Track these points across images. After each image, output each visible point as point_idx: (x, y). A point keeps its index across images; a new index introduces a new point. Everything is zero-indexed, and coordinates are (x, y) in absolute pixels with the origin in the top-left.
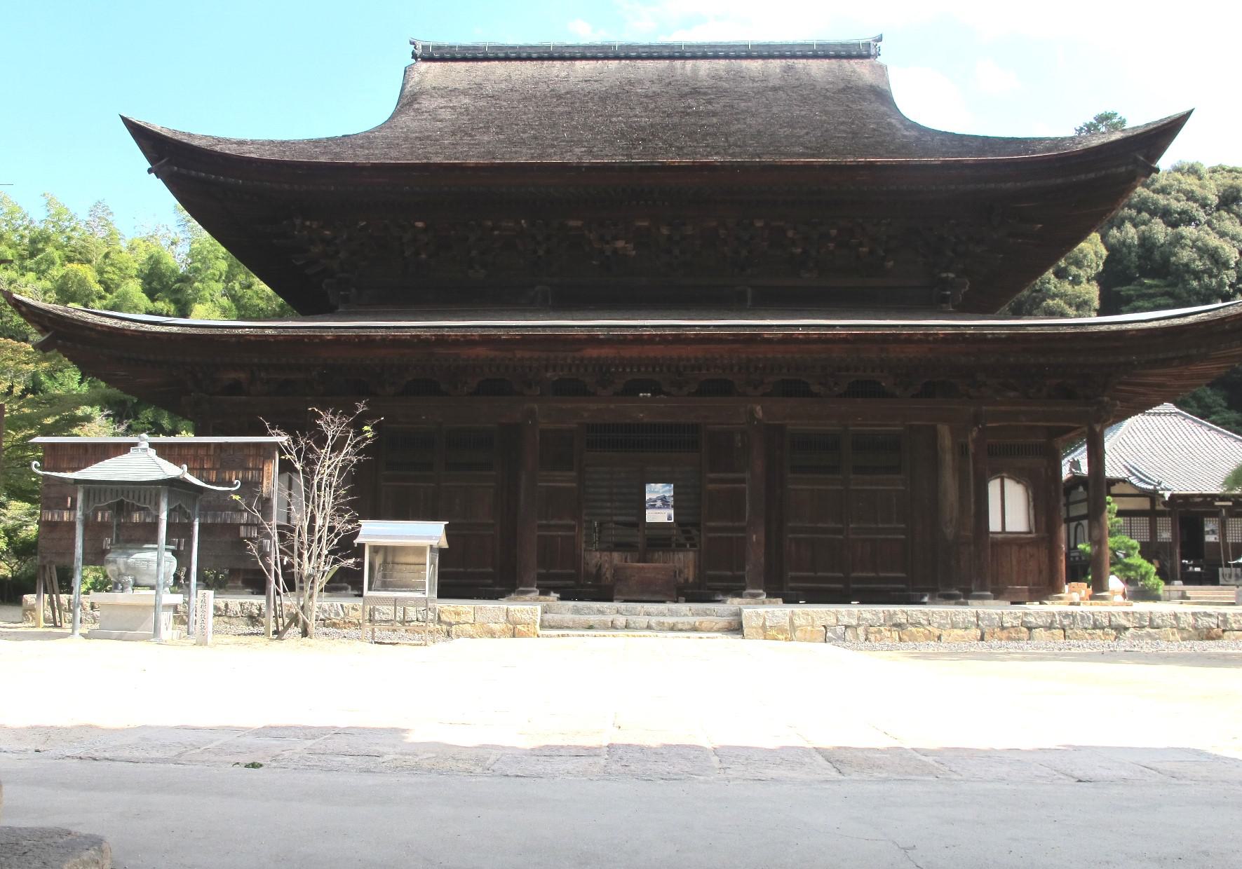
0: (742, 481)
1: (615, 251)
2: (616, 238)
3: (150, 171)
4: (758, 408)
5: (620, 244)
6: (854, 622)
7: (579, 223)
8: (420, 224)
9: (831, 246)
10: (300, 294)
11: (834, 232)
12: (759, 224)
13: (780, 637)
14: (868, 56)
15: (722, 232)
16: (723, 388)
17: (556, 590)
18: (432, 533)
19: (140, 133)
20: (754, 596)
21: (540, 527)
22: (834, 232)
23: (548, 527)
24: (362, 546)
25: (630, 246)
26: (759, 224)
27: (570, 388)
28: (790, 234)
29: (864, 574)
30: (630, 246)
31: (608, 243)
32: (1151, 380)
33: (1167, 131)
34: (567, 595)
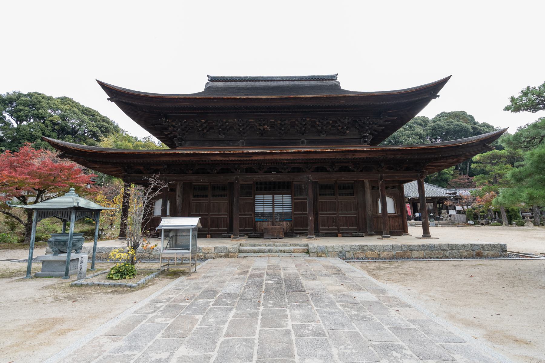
0: (306, 199)
1: (264, 129)
2: (264, 125)
3: (108, 99)
4: (310, 176)
5: (265, 127)
6: (349, 250)
7: (253, 121)
8: (203, 121)
9: (330, 126)
10: (172, 145)
11: (331, 122)
12: (308, 120)
13: (323, 255)
14: (334, 80)
15: (296, 122)
16: (298, 170)
17: (247, 234)
18: (193, 222)
19: (98, 81)
20: (311, 238)
21: (240, 215)
22: (331, 122)
23: (244, 215)
24: (160, 230)
25: (269, 128)
26: (308, 120)
27: (250, 171)
28: (318, 123)
29: (245, 159)
30: (269, 128)
31: (261, 126)
32: (438, 164)
33: (431, 91)
34: (250, 236)
